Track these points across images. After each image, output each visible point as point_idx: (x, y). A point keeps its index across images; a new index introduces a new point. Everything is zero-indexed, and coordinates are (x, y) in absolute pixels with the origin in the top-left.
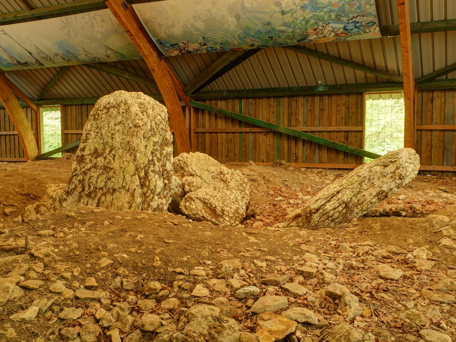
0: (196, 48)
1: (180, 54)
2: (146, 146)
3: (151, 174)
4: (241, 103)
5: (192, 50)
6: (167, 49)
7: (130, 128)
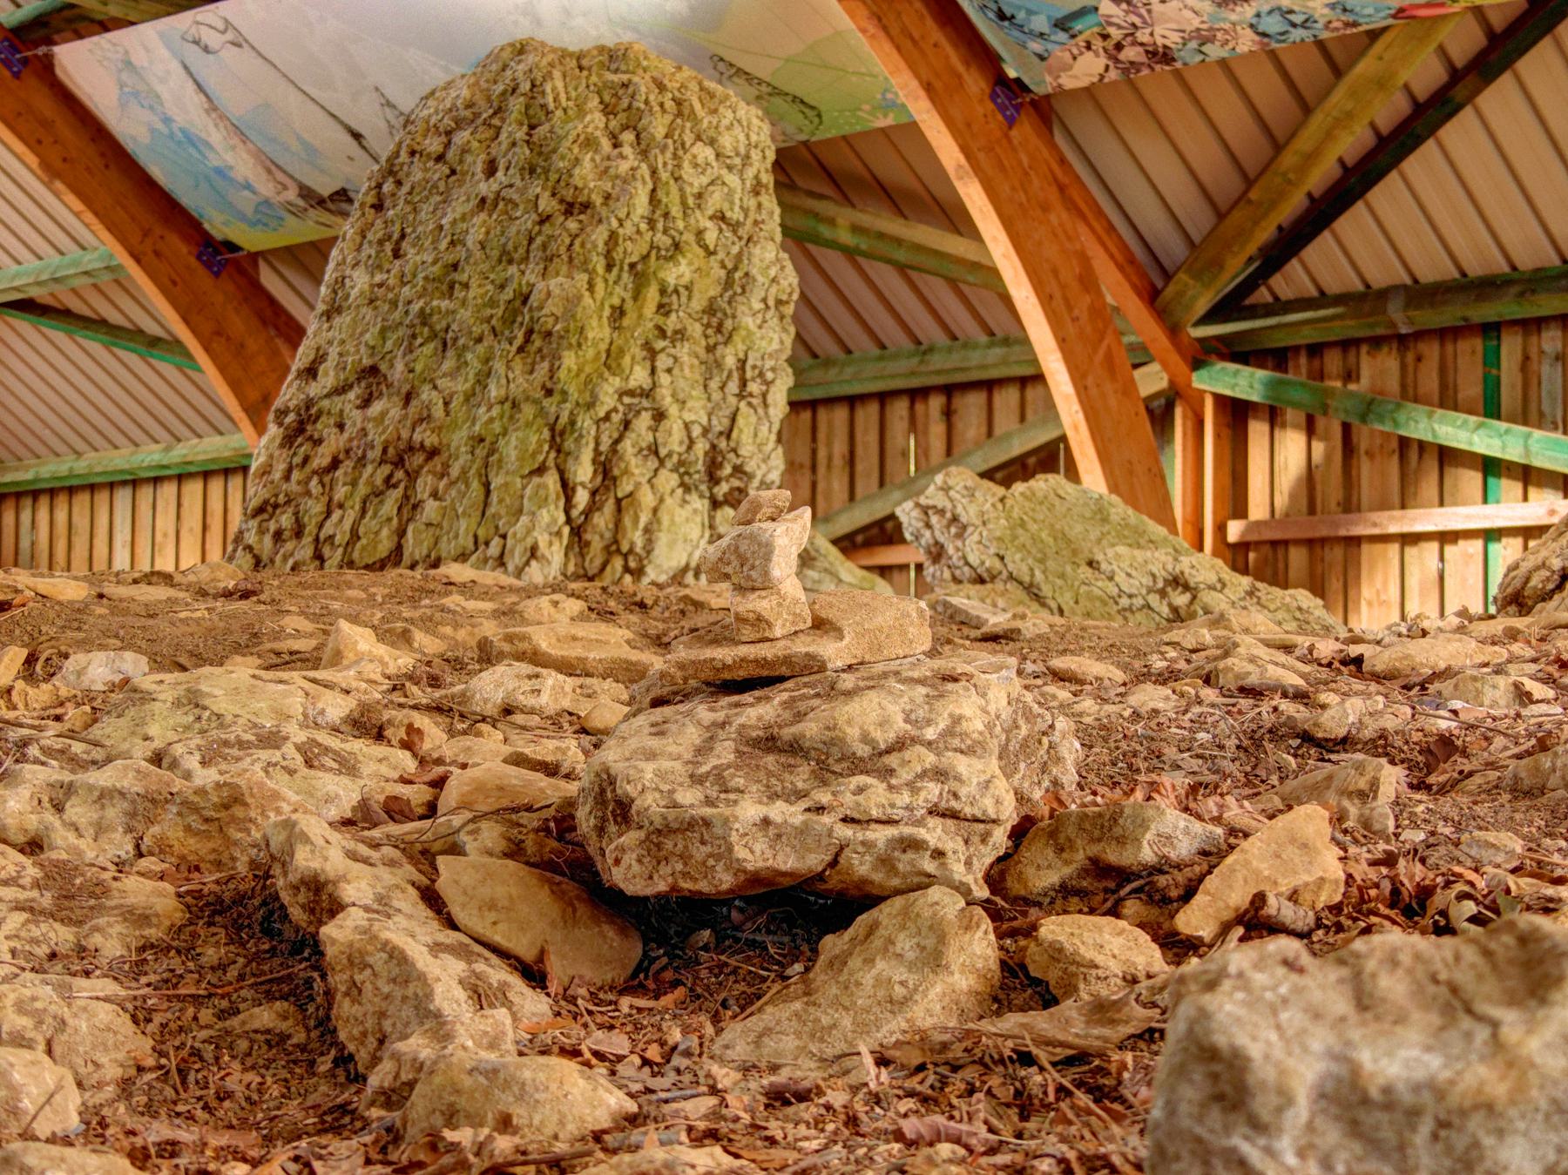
0: (1196, 23)
1: (1113, 75)
2: (619, 312)
3: (635, 470)
4: (1492, 361)
5: (1173, 39)
6: (1036, 46)
7: (544, 220)
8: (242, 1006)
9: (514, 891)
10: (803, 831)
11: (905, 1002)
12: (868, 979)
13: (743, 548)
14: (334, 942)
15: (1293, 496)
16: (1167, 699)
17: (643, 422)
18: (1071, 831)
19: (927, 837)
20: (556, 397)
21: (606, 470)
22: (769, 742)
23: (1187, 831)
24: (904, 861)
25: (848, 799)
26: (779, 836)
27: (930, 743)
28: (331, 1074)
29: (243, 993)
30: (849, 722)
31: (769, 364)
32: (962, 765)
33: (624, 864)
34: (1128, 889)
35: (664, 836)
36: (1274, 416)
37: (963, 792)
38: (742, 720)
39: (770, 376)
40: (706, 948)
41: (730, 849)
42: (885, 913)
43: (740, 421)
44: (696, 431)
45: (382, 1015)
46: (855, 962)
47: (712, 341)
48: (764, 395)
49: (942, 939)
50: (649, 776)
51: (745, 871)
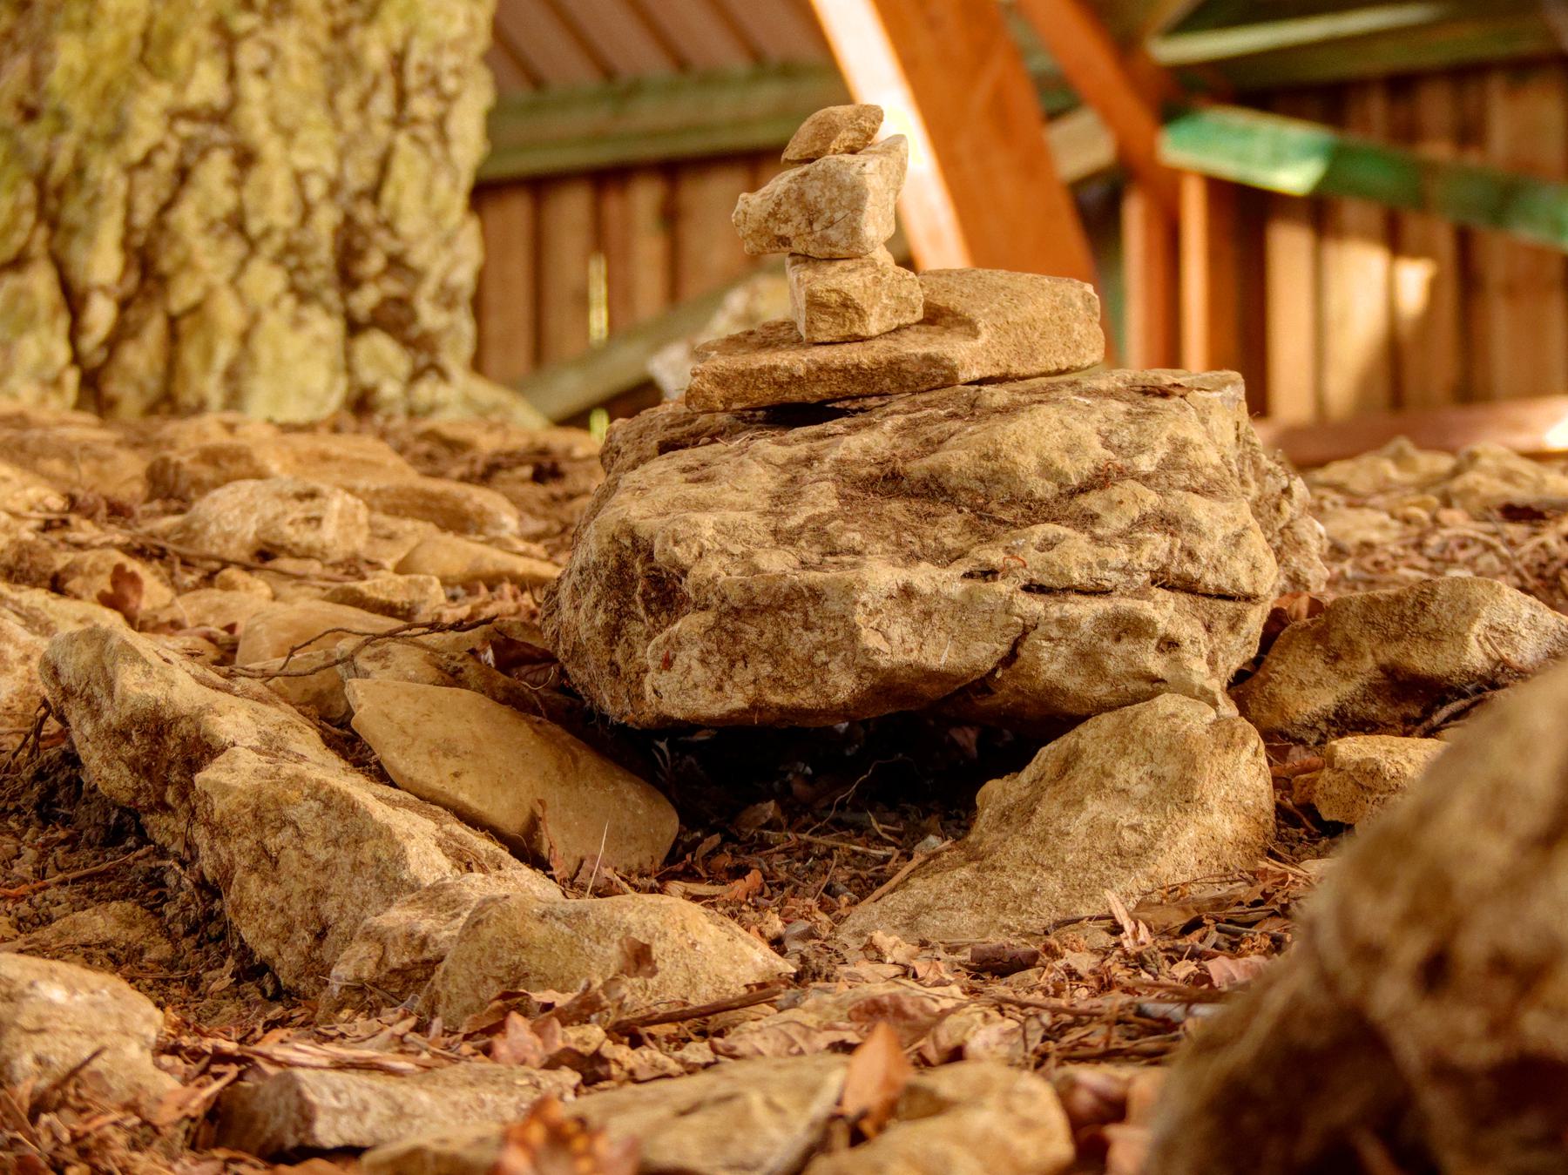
3: (204, 265)
8: (55, 911)
9: (477, 728)
10: (964, 607)
11: (1142, 853)
12: (1078, 826)
13: (811, 195)
14: (226, 790)
15: (1365, 385)
16: (1383, 527)
17: (216, 171)
18: (1351, 627)
19: (1155, 615)
20: (45, 124)
21: (147, 266)
22: (888, 481)
23: (1533, 623)
24: (1117, 657)
25: (1033, 557)
26: (928, 614)
27: (1146, 478)
28: (234, 993)
29: (52, 893)
30: (1019, 446)
31: (449, 60)
32: (1201, 509)
33: (678, 666)
34: (1445, 712)
35: (755, 612)
36: (1318, 213)
37: (1203, 549)
38: (839, 453)
39: (450, 84)
40: (772, 825)
41: (853, 634)
42: (1086, 736)
43: (399, 170)
44: (316, 188)
45: (320, 894)
46: (1049, 808)
47: (340, 17)
48: (441, 123)
49: (1190, 762)
50: (709, 533)
51: (874, 670)
